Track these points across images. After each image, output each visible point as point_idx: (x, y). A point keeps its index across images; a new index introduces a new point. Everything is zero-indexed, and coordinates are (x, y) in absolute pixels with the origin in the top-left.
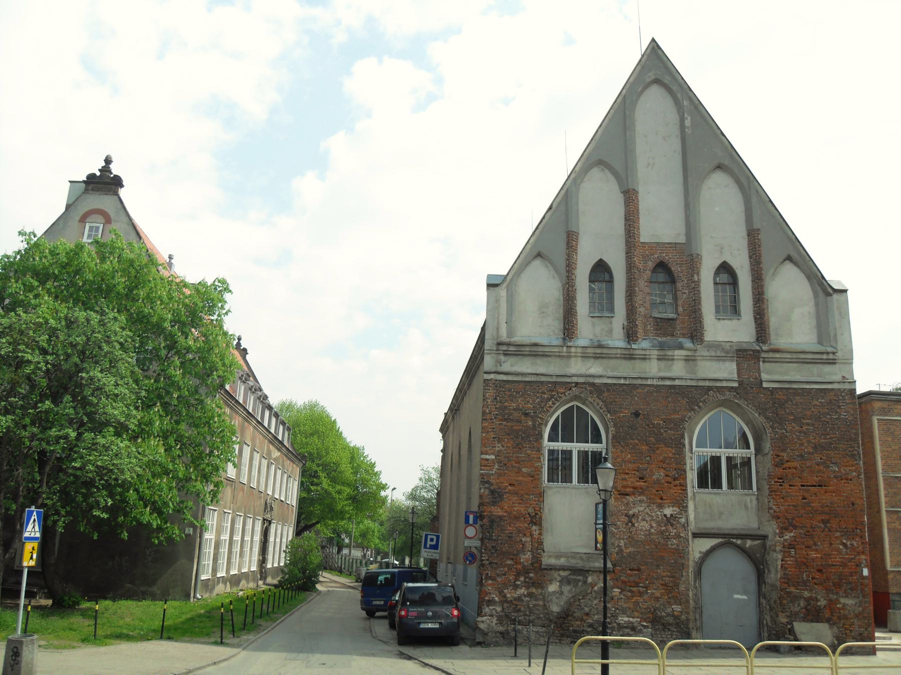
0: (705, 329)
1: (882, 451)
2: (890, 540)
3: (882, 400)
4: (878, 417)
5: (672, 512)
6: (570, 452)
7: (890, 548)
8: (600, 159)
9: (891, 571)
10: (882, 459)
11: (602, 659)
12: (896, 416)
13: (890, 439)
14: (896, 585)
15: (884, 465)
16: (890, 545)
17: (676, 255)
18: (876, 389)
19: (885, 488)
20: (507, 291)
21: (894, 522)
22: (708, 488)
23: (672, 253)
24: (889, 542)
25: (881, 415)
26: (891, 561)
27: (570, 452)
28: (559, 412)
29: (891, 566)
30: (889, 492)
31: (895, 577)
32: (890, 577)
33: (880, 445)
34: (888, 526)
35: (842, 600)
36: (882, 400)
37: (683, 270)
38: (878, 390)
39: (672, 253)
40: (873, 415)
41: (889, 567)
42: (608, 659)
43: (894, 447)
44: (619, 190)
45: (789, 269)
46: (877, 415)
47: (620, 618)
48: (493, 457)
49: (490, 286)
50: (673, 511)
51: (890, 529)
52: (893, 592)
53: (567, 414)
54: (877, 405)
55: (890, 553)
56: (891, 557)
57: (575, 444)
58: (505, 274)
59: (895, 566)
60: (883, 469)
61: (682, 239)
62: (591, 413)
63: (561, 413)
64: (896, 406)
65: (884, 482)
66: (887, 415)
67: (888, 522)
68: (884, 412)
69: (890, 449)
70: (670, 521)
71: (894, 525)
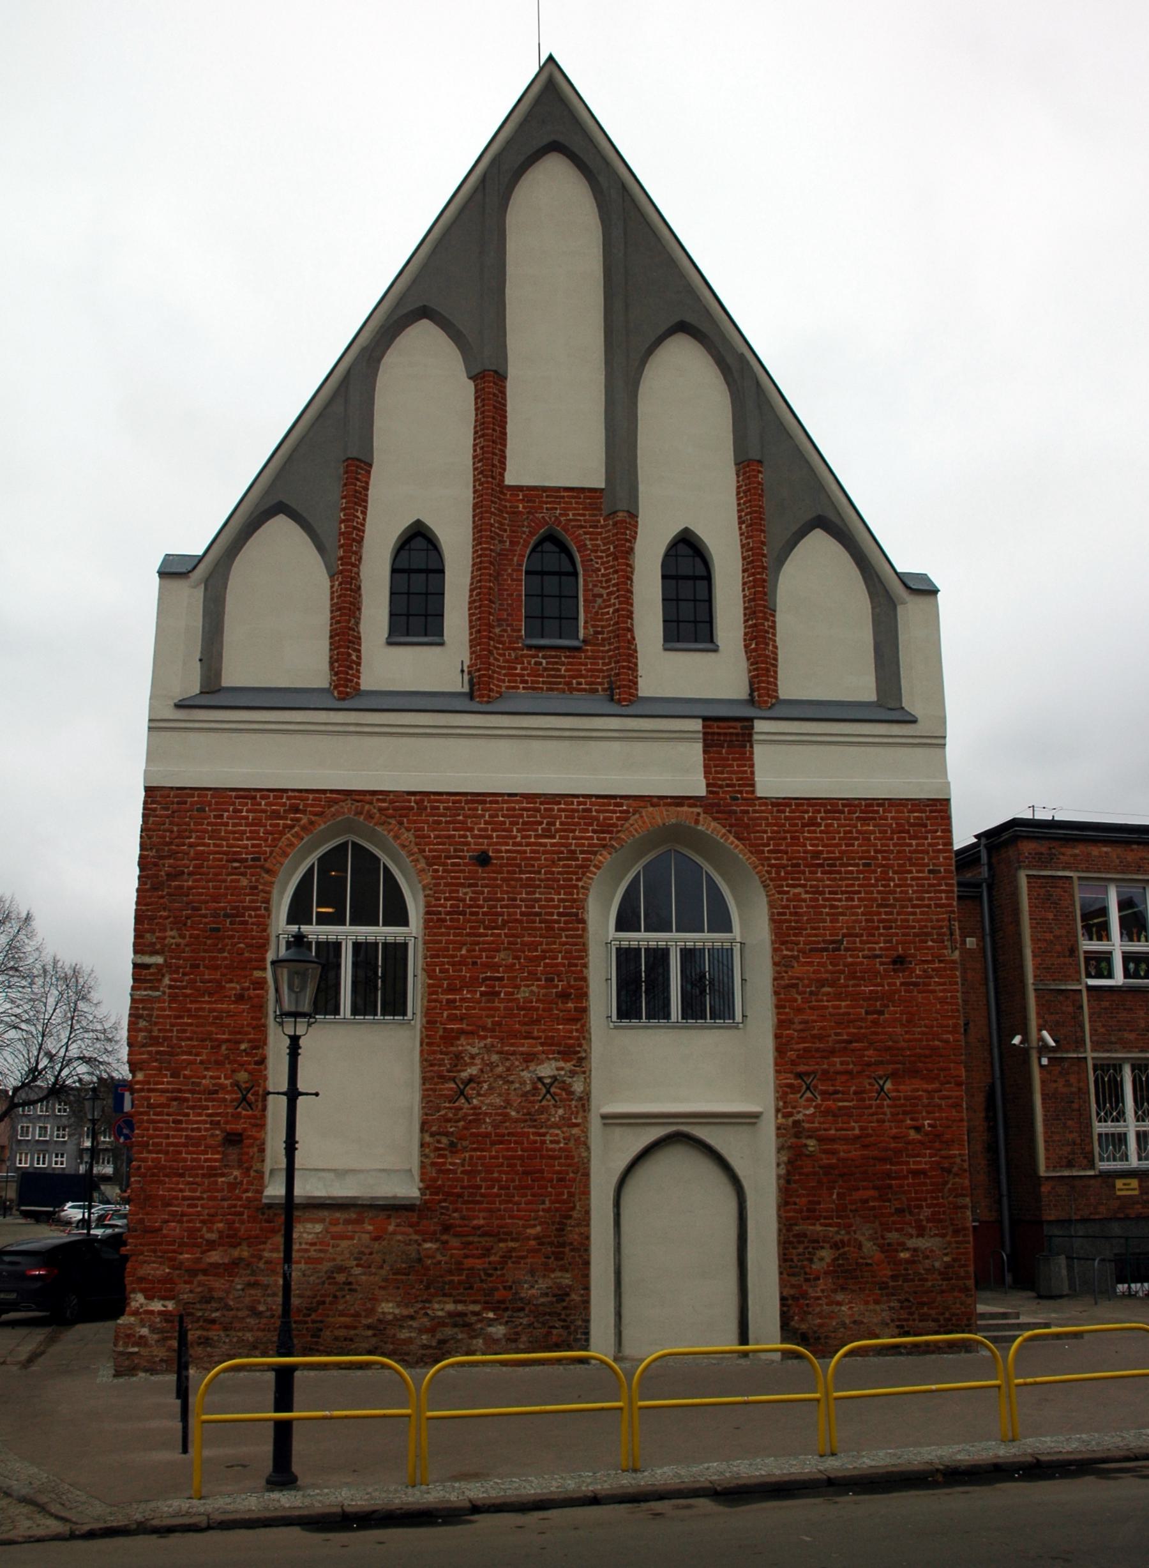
0: (640, 673)
1: (1035, 940)
2: (1046, 1115)
3: (1038, 838)
4: (1031, 873)
5: (556, 1073)
6: (337, 946)
7: (1045, 1133)
8: (425, 306)
9: (1048, 1178)
10: (1034, 956)
11: (277, 1410)
12: (1064, 869)
13: (1051, 916)
14: (1055, 1206)
15: (1038, 968)
16: (1045, 1125)
17: (584, 515)
18: (1028, 815)
19: (1038, 1014)
20: (206, 589)
21: (1055, 1081)
22: (641, 1018)
23: (575, 509)
24: (1044, 1120)
25: (1033, 867)
26: (1047, 1158)
27: (337, 946)
28: (313, 859)
29: (1047, 1167)
30: (1046, 1021)
31: (1053, 1188)
32: (1045, 1189)
33: (1031, 927)
34: (1042, 1090)
35: (912, 1243)
36: (1038, 838)
37: (598, 546)
38: (1031, 817)
39: (575, 509)
40: (1020, 867)
41: (1042, 1171)
42: (290, 1410)
43: (1057, 933)
44: (465, 375)
45: (818, 543)
46: (1028, 867)
47: (436, 1306)
48: (159, 960)
49: (163, 574)
50: (558, 1069)
51: (1048, 1095)
52: (1049, 1218)
53: (332, 860)
54: (1027, 847)
55: (1046, 1141)
56: (1046, 1149)
57: (348, 928)
58: (201, 553)
59: (1055, 1167)
60: (1035, 976)
61: (597, 480)
62: (385, 859)
63: (319, 859)
64: (1063, 850)
65: (1036, 1001)
66: (1045, 868)
67: (1043, 1082)
68: (1043, 861)
69: (1049, 936)
70: (557, 1089)
71: (1055, 1085)
